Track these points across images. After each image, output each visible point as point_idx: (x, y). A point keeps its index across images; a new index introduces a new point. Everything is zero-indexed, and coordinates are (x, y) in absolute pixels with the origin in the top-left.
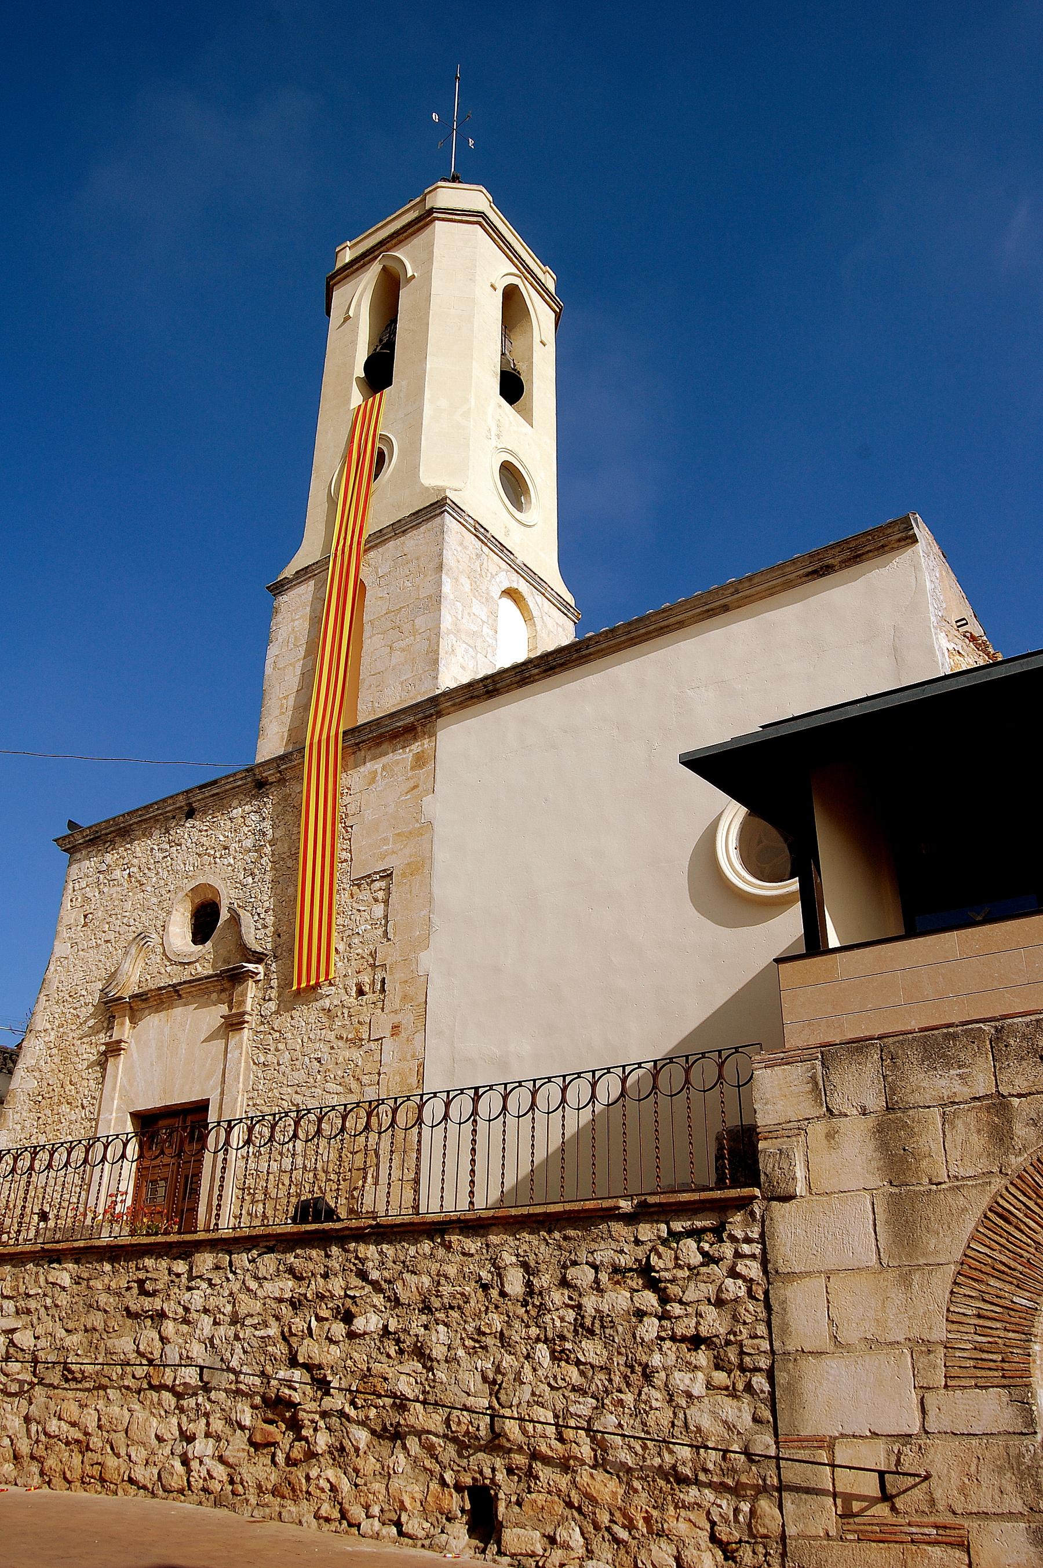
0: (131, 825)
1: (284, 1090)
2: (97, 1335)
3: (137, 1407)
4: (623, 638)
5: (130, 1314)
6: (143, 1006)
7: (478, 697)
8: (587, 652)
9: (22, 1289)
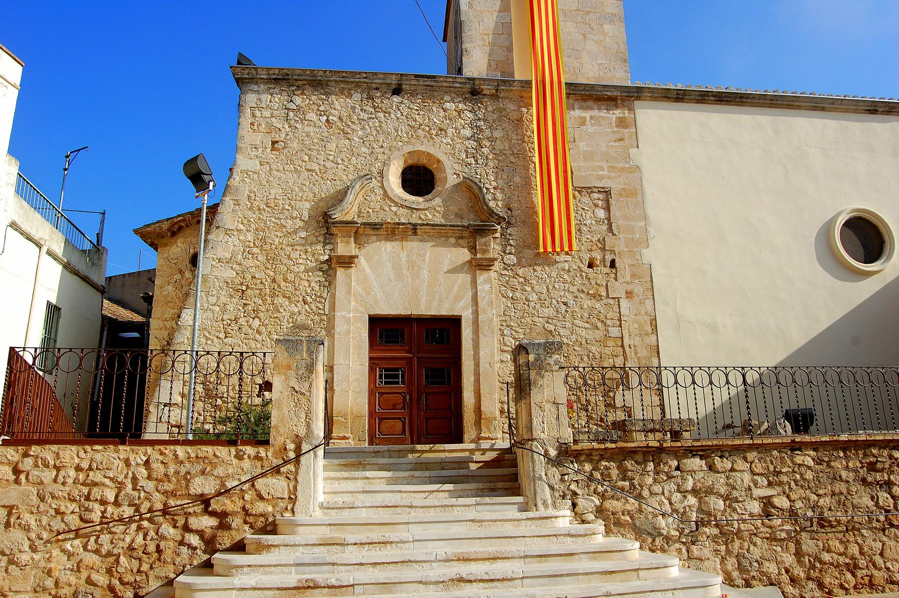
1: (536, 319)
2: (843, 498)
3: (885, 539)
5: (864, 481)
6: (371, 232)
9: (771, 468)
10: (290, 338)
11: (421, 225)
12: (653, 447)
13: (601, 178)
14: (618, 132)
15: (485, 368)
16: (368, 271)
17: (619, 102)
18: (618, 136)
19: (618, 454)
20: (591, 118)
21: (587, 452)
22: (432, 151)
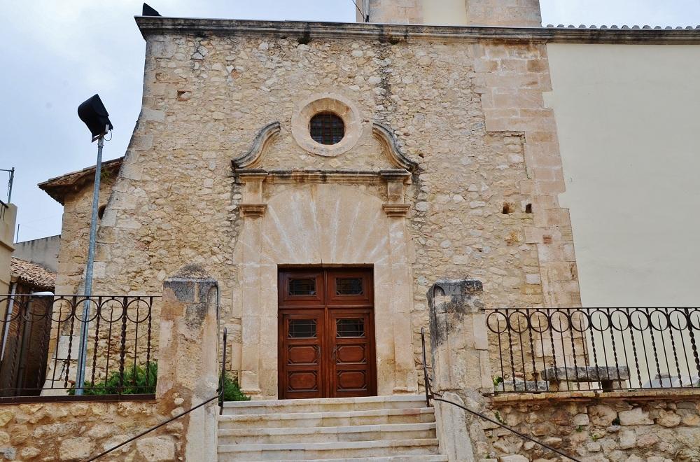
0: (237, 31)
4: (690, 38)
7: (583, 39)
8: (666, 38)
10: (180, 280)
11: (331, 172)
12: (587, 398)
13: (515, 122)
14: (531, 75)
15: (396, 313)
16: (277, 220)
17: (531, 45)
18: (531, 80)
19: (548, 406)
20: (503, 62)
21: (513, 404)
22: (339, 97)
